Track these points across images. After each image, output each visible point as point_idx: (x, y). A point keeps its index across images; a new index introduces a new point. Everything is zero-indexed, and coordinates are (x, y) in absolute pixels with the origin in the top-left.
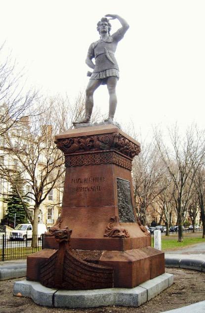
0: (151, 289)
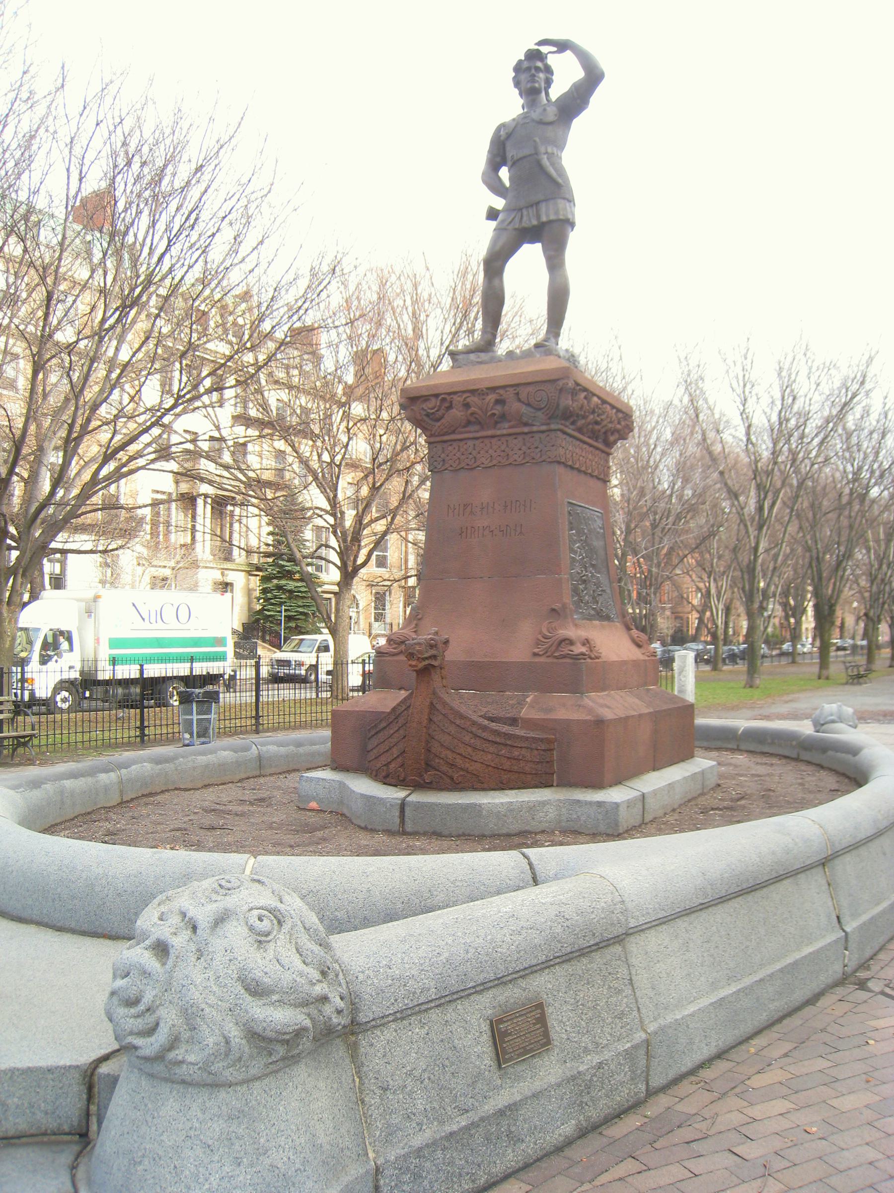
0: (655, 793)
